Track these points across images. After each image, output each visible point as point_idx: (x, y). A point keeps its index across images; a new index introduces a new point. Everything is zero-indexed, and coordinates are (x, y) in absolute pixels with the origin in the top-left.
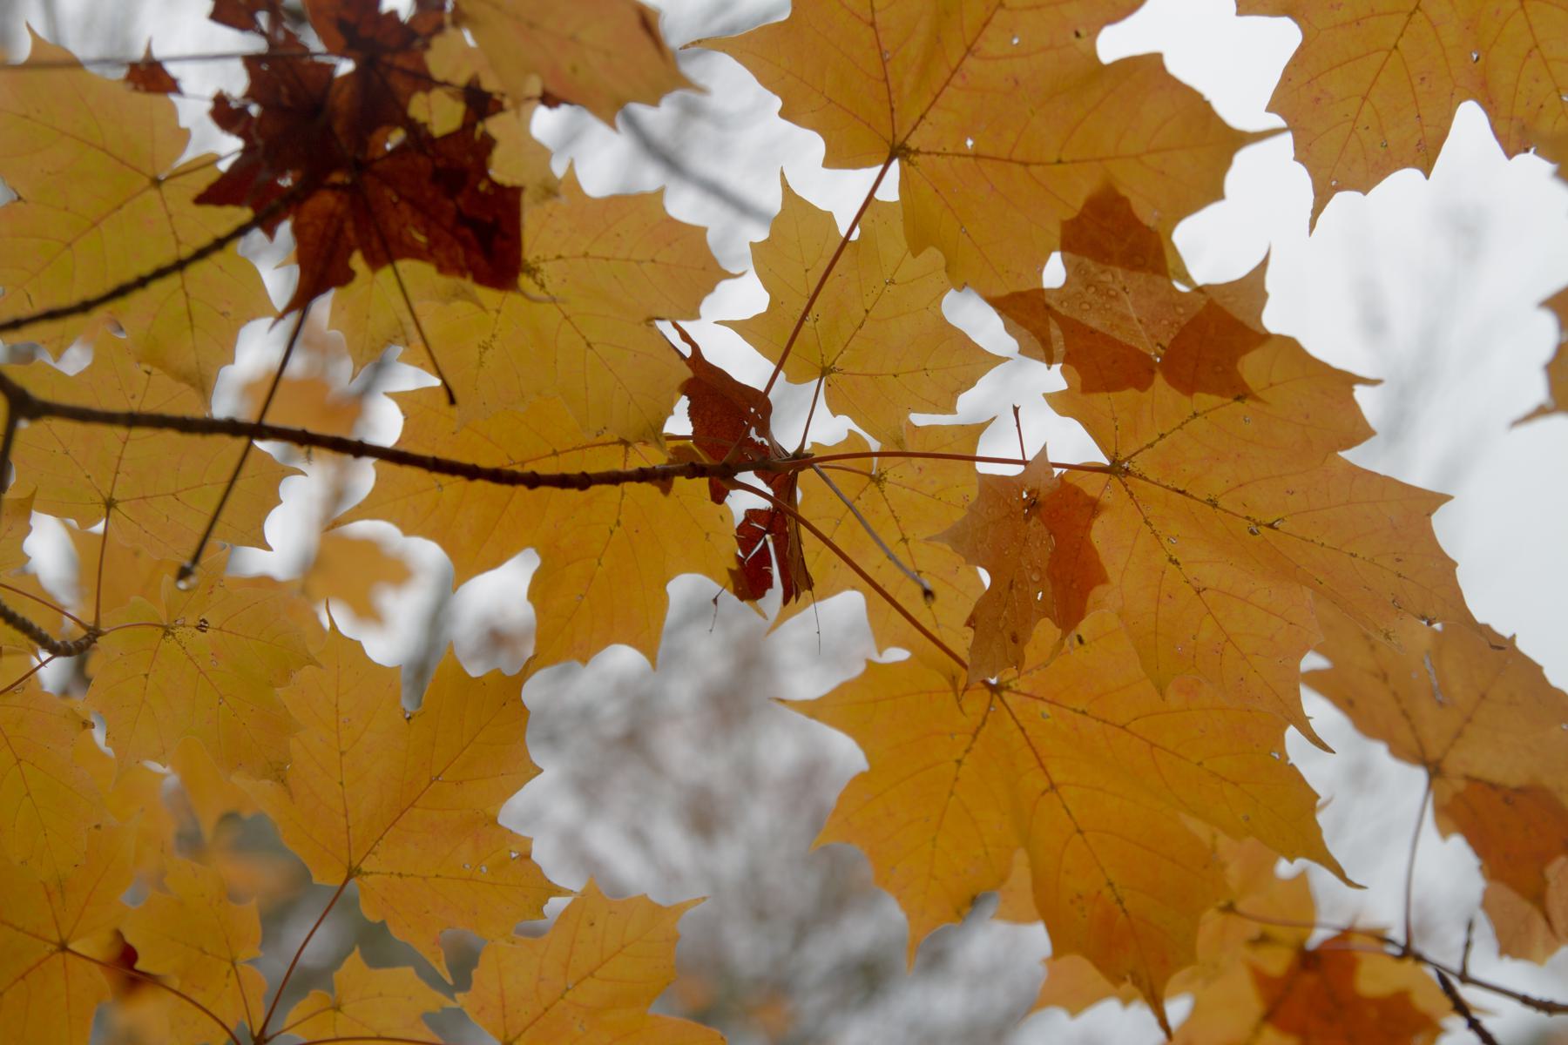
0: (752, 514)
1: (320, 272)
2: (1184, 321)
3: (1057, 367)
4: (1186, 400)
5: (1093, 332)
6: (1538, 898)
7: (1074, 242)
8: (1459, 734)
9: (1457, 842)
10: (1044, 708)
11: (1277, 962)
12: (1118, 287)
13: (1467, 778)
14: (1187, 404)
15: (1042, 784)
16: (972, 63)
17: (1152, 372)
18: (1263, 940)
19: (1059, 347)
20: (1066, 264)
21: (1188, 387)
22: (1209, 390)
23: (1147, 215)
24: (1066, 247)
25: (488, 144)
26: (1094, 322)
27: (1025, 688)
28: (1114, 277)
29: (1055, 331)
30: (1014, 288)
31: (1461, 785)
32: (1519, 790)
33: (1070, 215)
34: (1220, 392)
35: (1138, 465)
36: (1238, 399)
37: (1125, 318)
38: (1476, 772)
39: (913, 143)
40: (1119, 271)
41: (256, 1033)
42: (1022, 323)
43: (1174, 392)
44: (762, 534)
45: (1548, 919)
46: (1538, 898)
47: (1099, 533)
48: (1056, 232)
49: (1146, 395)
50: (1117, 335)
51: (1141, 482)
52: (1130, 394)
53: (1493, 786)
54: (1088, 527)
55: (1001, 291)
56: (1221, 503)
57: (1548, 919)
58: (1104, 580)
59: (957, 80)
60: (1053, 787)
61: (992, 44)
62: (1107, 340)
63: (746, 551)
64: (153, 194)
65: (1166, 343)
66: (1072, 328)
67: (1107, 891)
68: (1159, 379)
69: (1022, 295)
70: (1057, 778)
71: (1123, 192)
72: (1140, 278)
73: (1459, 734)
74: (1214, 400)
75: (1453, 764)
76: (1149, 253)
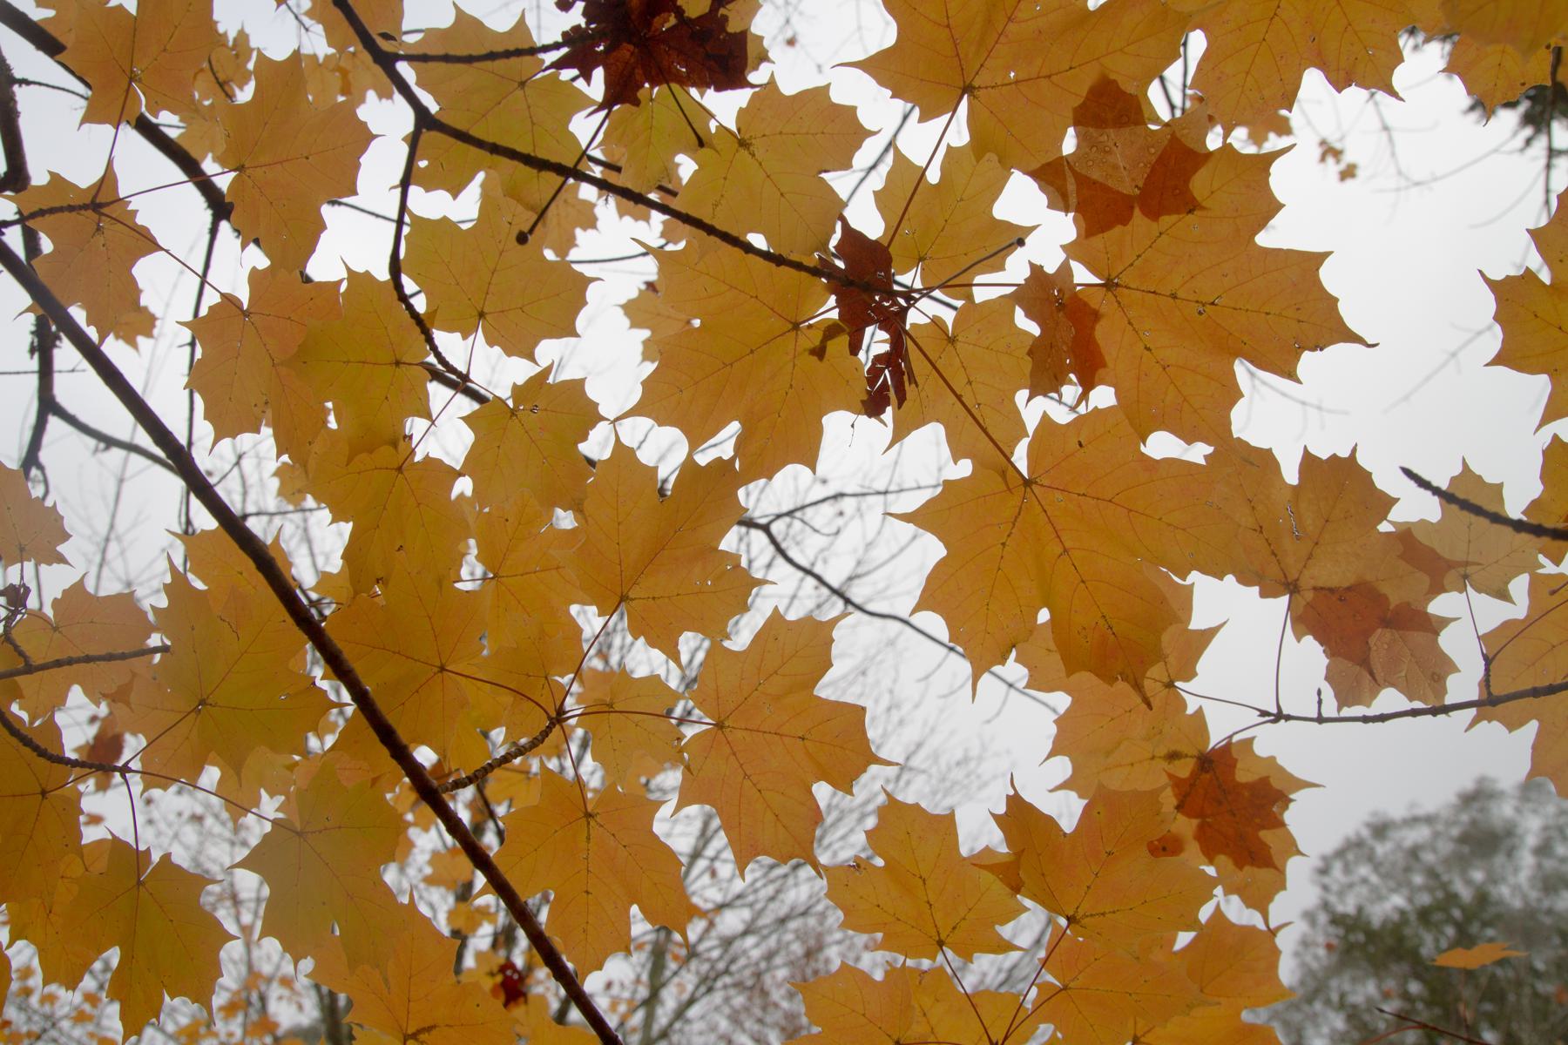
0: (877, 358)
1: (620, 92)
2: (1154, 159)
3: (1071, 215)
4: (1154, 225)
5: (1095, 183)
6: (1365, 662)
7: (1085, 118)
8: (1310, 557)
9: (1309, 640)
10: (1059, 495)
11: (1184, 769)
12: (1111, 144)
13: (1315, 589)
14: (1155, 228)
15: (1061, 550)
16: (1012, 27)
17: (1132, 208)
18: (1173, 756)
19: (1073, 200)
20: (1078, 135)
21: (1153, 214)
22: (1169, 213)
23: (1129, 88)
24: (1076, 124)
25: (725, 19)
26: (1096, 175)
27: (1046, 482)
28: (1110, 136)
29: (1071, 186)
30: (1044, 161)
31: (1309, 595)
32: (1349, 589)
33: (1078, 102)
34: (1178, 212)
35: (1123, 280)
36: (1190, 212)
37: (1116, 167)
38: (1320, 584)
39: (976, 84)
40: (1111, 131)
41: (604, 113)
42: (1050, 183)
43: (1146, 220)
44: (882, 371)
45: (1372, 674)
46: (1365, 662)
47: (1100, 332)
48: (1070, 115)
49: (1129, 227)
50: (1110, 183)
51: (1126, 291)
52: (1118, 229)
53: (1331, 590)
54: (1093, 328)
55: (1035, 165)
56: (1180, 294)
57: (1372, 674)
58: (1104, 365)
59: (1002, 39)
60: (1065, 550)
61: (1021, 15)
62: (1105, 189)
63: (872, 386)
64: (519, 93)
65: (1141, 184)
66: (1083, 181)
67: (1102, 622)
68: (1137, 212)
69: (1049, 164)
70: (1067, 545)
71: (1113, 76)
72: (1126, 131)
73: (1310, 557)
74: (1174, 218)
75: (1306, 582)
76: (1131, 110)
